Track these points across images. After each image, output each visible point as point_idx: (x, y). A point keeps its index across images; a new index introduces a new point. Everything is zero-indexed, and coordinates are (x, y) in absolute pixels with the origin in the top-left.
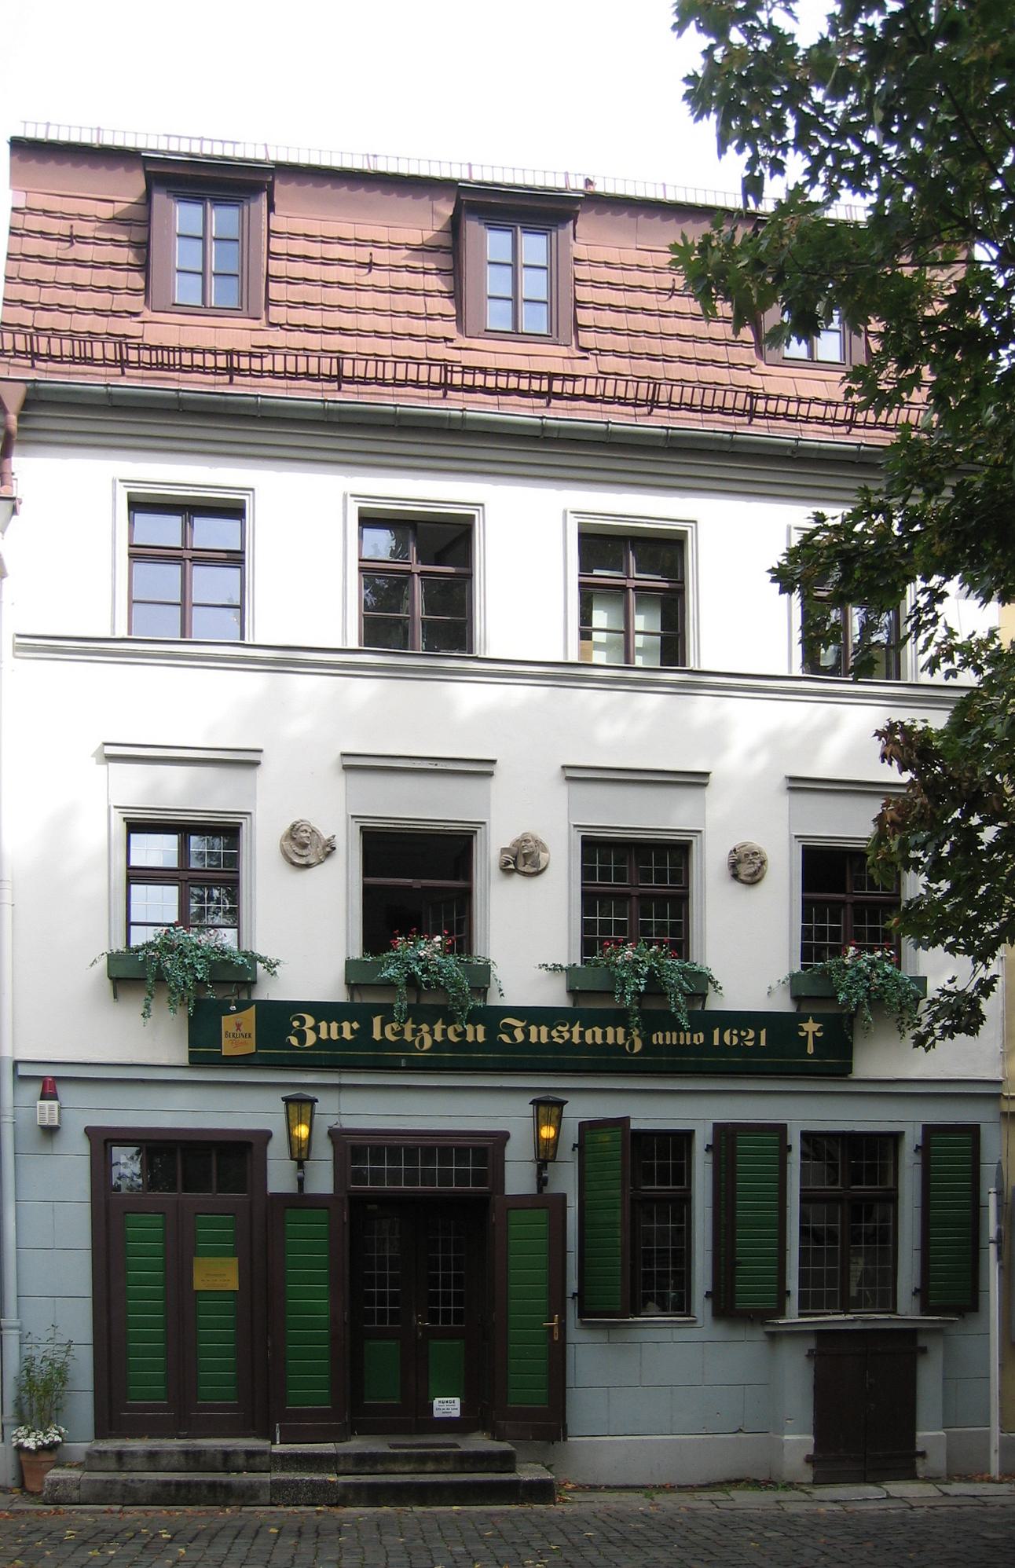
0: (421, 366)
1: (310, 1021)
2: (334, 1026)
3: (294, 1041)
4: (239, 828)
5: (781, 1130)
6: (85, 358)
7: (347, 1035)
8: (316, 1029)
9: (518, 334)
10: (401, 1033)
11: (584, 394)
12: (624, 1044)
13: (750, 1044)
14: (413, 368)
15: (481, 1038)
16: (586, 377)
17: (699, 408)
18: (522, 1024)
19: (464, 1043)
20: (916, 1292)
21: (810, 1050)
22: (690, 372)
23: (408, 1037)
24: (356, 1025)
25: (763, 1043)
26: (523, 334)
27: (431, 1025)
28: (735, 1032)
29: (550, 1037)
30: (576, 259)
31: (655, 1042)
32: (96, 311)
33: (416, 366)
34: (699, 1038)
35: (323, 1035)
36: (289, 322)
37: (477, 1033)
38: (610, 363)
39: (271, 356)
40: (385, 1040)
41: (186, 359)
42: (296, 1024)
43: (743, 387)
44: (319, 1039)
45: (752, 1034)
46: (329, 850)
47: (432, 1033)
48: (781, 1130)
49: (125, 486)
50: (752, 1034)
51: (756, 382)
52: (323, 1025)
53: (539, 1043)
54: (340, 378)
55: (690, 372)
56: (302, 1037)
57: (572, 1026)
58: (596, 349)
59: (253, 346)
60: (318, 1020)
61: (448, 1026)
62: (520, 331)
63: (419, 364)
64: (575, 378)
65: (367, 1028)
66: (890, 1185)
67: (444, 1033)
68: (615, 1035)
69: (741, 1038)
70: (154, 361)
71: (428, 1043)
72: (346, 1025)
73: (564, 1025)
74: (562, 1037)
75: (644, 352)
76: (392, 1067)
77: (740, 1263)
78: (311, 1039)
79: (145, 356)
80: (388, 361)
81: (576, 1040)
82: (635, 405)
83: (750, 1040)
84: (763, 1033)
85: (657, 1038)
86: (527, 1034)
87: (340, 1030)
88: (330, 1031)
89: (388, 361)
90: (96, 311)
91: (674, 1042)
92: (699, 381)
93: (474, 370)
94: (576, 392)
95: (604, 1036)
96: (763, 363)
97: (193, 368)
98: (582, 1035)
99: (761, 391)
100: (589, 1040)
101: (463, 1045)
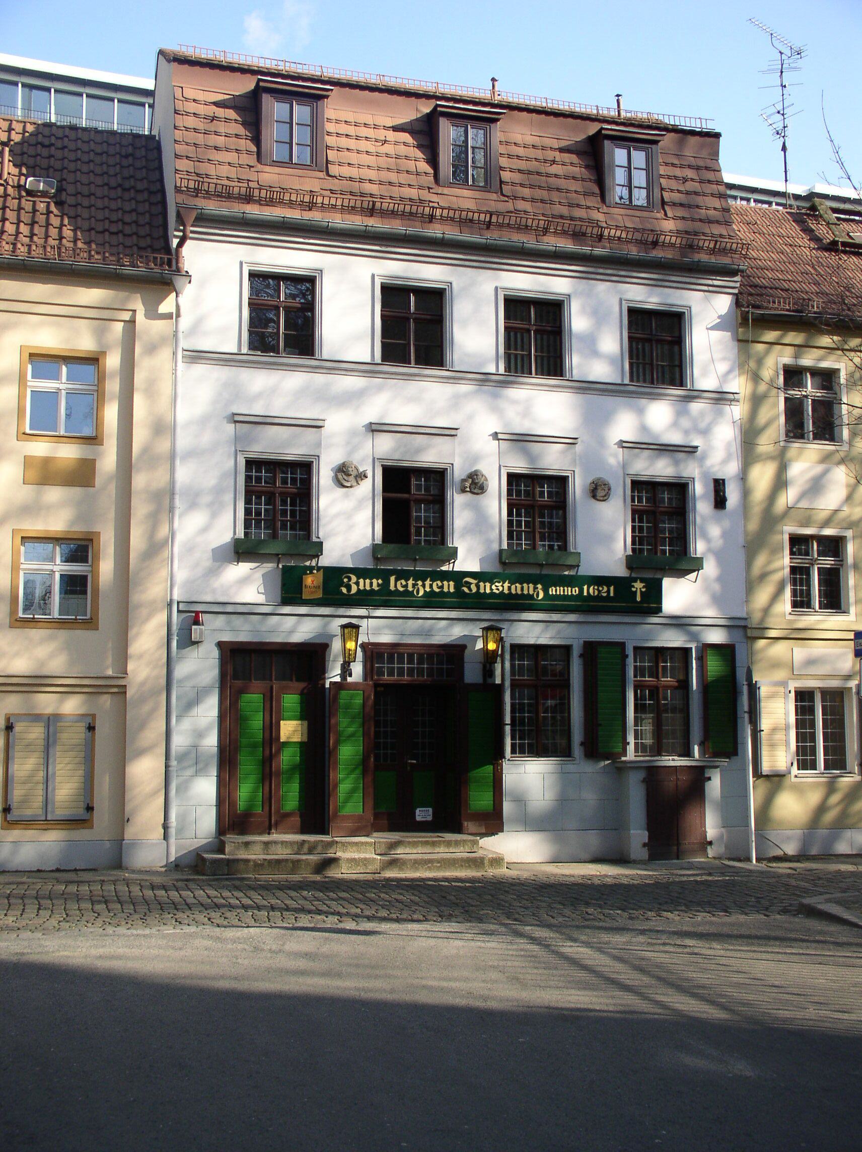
1: (354, 578)
2: (368, 581)
3: (344, 590)
5: (622, 645)
8: (357, 583)
10: (406, 586)
12: (413, 591)
15: (452, 590)
18: (476, 582)
23: (410, 589)
25: (612, 594)
27: (424, 580)
34: (575, 592)
37: (449, 587)
44: (359, 589)
46: (362, 476)
47: (424, 586)
48: (622, 645)
56: (349, 588)
57: (504, 583)
60: (358, 578)
61: (433, 582)
65: (387, 582)
67: (431, 586)
68: (528, 589)
69: (599, 591)
71: (421, 593)
72: (375, 581)
73: (499, 582)
78: (354, 589)
85: (552, 591)
86: (478, 586)
87: (371, 584)
88: (365, 584)
95: (522, 589)
98: (509, 588)
101: (442, 594)
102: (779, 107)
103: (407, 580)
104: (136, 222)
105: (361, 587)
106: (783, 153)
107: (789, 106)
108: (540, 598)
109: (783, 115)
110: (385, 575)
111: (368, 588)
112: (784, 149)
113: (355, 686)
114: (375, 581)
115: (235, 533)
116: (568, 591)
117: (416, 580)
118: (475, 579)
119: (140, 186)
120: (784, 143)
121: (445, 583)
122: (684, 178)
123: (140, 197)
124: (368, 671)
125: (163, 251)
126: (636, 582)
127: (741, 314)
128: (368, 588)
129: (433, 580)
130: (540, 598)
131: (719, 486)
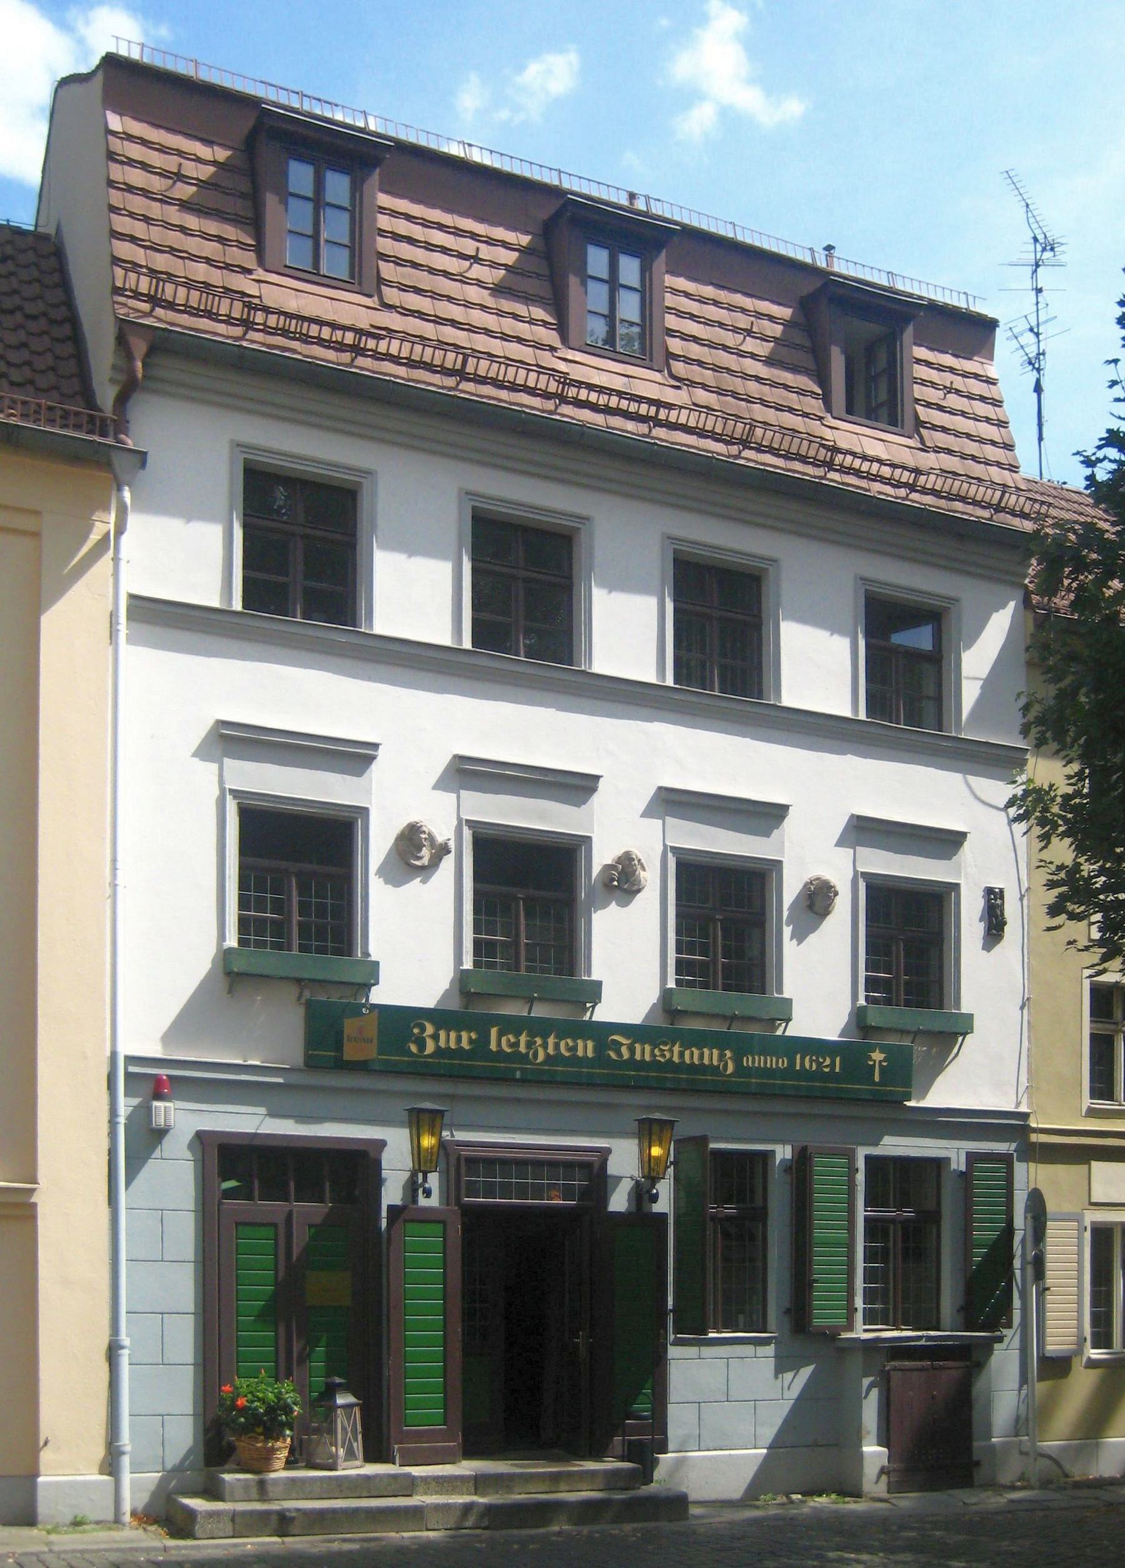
0: (541, 376)
1: (430, 1029)
2: (453, 1035)
3: (414, 1048)
4: (575, 850)
6: (210, 312)
7: (465, 1044)
8: (435, 1037)
9: (320, 275)
10: (516, 1044)
11: (686, 425)
12: (528, 1054)
13: (827, 1070)
14: (522, 373)
15: (590, 1054)
16: (681, 407)
17: (261, 327)
18: (628, 1042)
19: (575, 1057)
20: (788, 1312)
21: (877, 1079)
22: (496, 346)
23: (522, 1049)
24: (473, 1036)
25: (837, 1070)
26: (325, 276)
27: (545, 1038)
28: (814, 1058)
29: (653, 1055)
30: (380, 207)
31: (745, 1064)
32: (208, 261)
33: (526, 371)
34: (783, 1063)
35: (442, 1044)
36: (403, 305)
37: (586, 1048)
38: (702, 396)
39: (388, 339)
40: (500, 1051)
41: (314, 330)
42: (416, 1031)
43: (817, 437)
44: (438, 1048)
45: (828, 1062)
47: (545, 1046)
49: (470, 499)
50: (828, 1062)
51: (252, 289)
52: (442, 1034)
53: (643, 1061)
54: (460, 374)
55: (496, 346)
56: (422, 1045)
57: (673, 1045)
58: (688, 380)
59: (372, 326)
60: (438, 1028)
61: (561, 1039)
62: (322, 273)
63: (529, 370)
64: (670, 406)
65: (485, 1039)
66: (759, 1202)
67: (557, 1046)
69: (819, 1064)
70: (202, 308)
71: (541, 1057)
72: (464, 1035)
73: (665, 1044)
74: (663, 1056)
75: (729, 389)
76: (506, 1079)
77: (816, 1281)
78: (430, 1047)
79: (272, 320)
80: (533, 370)
81: (676, 1059)
82: (727, 443)
83: (827, 1066)
84: (838, 1059)
85: (748, 1061)
86: (632, 1050)
87: (459, 1039)
88: (449, 1039)
89: (533, 370)
90: (208, 261)
91: (696, 1061)
92: (438, 341)
93: (579, 384)
94: (579, 398)
95: (701, 1056)
96: (829, 415)
97: (320, 342)
98: (681, 1054)
99: (256, 301)
100: (687, 1060)
101: (574, 1060)
102: (1034, 323)
103: (518, 1035)
104: (28, 363)
105: (442, 1044)
106: (1035, 395)
107: (1047, 321)
108: (728, 1073)
109: (1037, 335)
110: (482, 1024)
111: (453, 1045)
112: (1038, 389)
113: (427, 1217)
114: (464, 1035)
115: (222, 936)
116: (772, 1062)
117: (532, 1035)
118: (627, 1037)
119: (31, 308)
120: (1038, 382)
121: (580, 1043)
122: (945, 387)
123: (32, 326)
124: (452, 1191)
125: (78, 398)
126: (874, 1051)
127: (1035, 620)
128: (453, 1045)
129: (560, 1037)
130: (728, 1073)
131: (994, 900)
